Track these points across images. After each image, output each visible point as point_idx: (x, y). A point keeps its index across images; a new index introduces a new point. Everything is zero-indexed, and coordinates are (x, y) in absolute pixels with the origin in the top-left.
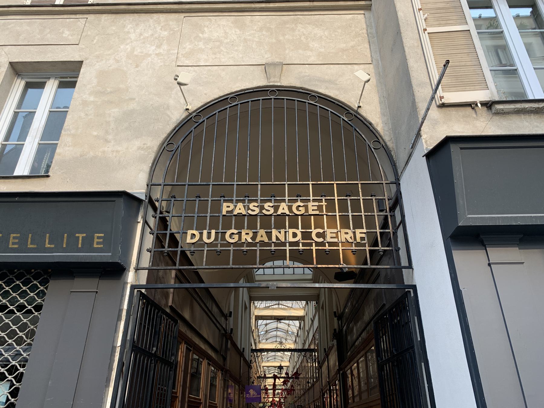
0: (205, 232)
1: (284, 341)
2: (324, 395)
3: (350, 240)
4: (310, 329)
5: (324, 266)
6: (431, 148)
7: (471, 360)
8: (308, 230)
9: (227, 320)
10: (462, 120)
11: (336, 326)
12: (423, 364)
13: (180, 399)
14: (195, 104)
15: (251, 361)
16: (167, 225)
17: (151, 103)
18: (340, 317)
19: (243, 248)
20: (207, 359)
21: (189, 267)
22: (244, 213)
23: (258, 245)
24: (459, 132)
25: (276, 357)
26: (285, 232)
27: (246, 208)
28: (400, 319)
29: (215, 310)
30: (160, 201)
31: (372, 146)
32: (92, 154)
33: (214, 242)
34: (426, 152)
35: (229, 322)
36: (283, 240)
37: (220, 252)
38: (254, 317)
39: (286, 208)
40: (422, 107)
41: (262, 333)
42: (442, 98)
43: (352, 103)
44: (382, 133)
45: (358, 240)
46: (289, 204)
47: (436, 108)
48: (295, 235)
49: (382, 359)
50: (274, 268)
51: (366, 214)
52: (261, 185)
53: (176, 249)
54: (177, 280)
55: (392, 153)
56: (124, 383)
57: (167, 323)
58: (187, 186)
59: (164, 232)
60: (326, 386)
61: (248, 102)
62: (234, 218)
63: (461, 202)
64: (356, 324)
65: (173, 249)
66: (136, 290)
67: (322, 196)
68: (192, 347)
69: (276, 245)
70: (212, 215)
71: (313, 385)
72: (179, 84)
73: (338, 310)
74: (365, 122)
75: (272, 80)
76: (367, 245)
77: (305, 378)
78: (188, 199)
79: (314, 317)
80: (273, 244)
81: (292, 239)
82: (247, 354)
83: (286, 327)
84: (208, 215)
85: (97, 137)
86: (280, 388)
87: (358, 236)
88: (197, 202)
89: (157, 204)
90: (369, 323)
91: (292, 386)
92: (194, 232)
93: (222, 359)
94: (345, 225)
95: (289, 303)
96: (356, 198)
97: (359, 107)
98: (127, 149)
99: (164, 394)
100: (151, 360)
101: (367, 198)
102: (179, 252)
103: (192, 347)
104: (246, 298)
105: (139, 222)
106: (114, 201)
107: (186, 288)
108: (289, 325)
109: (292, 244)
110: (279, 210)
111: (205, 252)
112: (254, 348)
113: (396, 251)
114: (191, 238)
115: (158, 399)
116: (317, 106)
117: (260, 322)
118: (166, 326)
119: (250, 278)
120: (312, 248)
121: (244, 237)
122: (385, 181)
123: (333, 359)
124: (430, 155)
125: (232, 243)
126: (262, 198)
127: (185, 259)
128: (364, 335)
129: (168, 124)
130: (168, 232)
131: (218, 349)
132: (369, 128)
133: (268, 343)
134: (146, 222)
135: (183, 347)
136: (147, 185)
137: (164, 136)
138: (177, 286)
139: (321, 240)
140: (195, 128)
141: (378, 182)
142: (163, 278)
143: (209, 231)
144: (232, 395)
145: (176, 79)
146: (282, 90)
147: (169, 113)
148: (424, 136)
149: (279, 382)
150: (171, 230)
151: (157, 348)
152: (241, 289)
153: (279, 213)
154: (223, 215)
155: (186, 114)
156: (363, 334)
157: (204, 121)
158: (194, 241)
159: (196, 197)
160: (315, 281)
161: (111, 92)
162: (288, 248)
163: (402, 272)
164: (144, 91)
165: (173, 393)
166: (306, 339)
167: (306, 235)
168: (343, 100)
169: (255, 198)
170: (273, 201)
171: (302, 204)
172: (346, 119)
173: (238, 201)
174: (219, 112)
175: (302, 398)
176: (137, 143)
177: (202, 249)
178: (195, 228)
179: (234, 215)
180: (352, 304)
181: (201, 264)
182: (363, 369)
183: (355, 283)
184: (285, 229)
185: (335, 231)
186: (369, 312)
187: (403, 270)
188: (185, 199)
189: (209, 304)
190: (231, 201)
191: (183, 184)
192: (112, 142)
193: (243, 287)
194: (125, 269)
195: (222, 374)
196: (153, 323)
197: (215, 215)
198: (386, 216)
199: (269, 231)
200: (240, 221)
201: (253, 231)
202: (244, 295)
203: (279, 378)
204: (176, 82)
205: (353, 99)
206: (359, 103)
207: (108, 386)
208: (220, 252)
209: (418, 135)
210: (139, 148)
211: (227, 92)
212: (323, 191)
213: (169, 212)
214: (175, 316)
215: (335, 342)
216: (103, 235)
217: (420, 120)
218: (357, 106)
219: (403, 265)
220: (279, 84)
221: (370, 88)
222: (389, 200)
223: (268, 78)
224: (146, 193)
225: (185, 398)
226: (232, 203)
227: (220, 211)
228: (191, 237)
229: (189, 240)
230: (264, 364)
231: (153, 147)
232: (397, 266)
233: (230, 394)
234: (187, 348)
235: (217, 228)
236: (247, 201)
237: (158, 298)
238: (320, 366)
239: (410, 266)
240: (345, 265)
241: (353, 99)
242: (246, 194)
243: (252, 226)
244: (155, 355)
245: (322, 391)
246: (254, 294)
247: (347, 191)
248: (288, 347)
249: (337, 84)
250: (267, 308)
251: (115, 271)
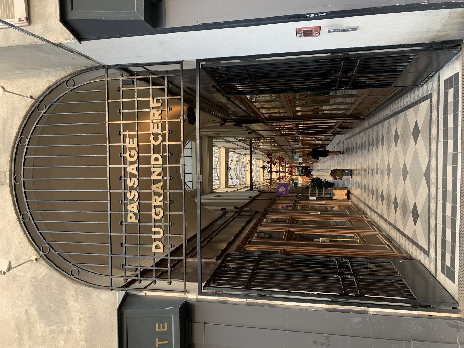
0: (154, 237)
1: (244, 165)
2: (283, 135)
3: (160, 112)
4: (235, 144)
5: (182, 136)
6: (72, 36)
7: (253, 23)
8: (152, 148)
9: (227, 212)
10: (43, 4)
11: (232, 124)
12: (257, 59)
13: (285, 247)
14: (30, 252)
15: (259, 191)
16: (148, 269)
17: (30, 294)
18: (225, 121)
19: (168, 204)
20: (257, 227)
21: (184, 248)
22: (137, 204)
23: (165, 191)
24: (56, 7)
25: (256, 170)
26: (154, 167)
27: (132, 202)
28: (223, 74)
29: (220, 222)
30: (126, 278)
31: (72, 88)
32: (82, 343)
33: (163, 228)
34: (76, 40)
35: (229, 210)
36: (161, 169)
37: (172, 223)
38: (226, 189)
39: (132, 167)
40: (30, 40)
41: (238, 182)
42: (20, 20)
43: (27, 104)
44: (59, 78)
45: (159, 105)
46: (128, 164)
48: (156, 159)
49: (254, 91)
50: (184, 174)
51: (136, 96)
52: (110, 189)
53: (169, 261)
54: (195, 257)
55: (79, 69)
56: (273, 293)
57: (229, 262)
58: (112, 256)
59: (154, 272)
60: (276, 133)
61: (27, 202)
62: (141, 213)
63: (123, 15)
64: (229, 109)
65: (169, 263)
67: (120, 135)
68: (247, 240)
69: (165, 175)
70: (139, 232)
71: (276, 142)
72: (9, 269)
73: (219, 122)
74: (48, 92)
75: (3, 180)
76: (163, 98)
77: (271, 148)
78: (124, 253)
79: (225, 140)
80: (165, 178)
81: (160, 162)
82: (254, 194)
83: (234, 163)
84: (139, 235)
85: (66, 340)
86: (278, 167)
87: (155, 105)
88: (127, 245)
89: (129, 280)
90: (228, 98)
91: (277, 159)
92: (154, 246)
93: (257, 215)
94: (146, 115)
95: (215, 161)
96: (121, 104)
97: (31, 97)
98: (77, 312)
99: (282, 260)
100: (257, 273)
101: (121, 95)
102: (172, 258)
103: (247, 240)
104: (211, 196)
105: (146, 294)
106: (127, 318)
107: (201, 248)
108: (232, 161)
109: (164, 162)
110: (133, 173)
111: (171, 235)
112: (249, 188)
113: (168, 73)
114: (160, 248)
115: (285, 265)
116: (31, 137)
117: (230, 184)
118: (232, 262)
119: (193, 194)
120: (167, 145)
121: (158, 203)
122: (105, 78)
123: (256, 127)
124: (80, 38)
125: (164, 213)
126: (123, 188)
127: (176, 252)
128: (237, 103)
129: (52, 276)
130: (154, 268)
131: (249, 218)
132: (54, 89)
134: (146, 288)
135: (248, 247)
136: (112, 290)
137: (64, 279)
138: (199, 257)
139: (160, 137)
140: (56, 251)
141: (106, 84)
142: (193, 268)
143: (153, 233)
144: (284, 205)
145: (4, 273)
146: (14, 170)
147: (40, 277)
148: (60, 40)
149: (274, 168)
150: (152, 266)
151: (248, 269)
152: (202, 201)
153: (136, 173)
154: (139, 222)
155: (42, 262)
156: (236, 103)
157: (48, 243)
158: (162, 246)
159: (122, 246)
160: (195, 140)
161: (19, 333)
162: (167, 165)
163: (186, 70)
164: (17, 302)
165: (281, 254)
166: (243, 147)
167: (156, 149)
168: (24, 112)
169: (123, 195)
170: (126, 178)
171: (128, 153)
172: (45, 110)
173: (126, 210)
174: (38, 230)
175: (286, 151)
176: (72, 303)
177: (169, 238)
178: (150, 246)
179: (139, 212)
180: (214, 111)
181: (181, 238)
182: (263, 103)
183: (195, 106)
184: (151, 167)
185: (152, 124)
186: (220, 98)
187: (184, 68)
188: (124, 256)
189: (215, 227)
190: (126, 216)
191: (110, 259)
192: (70, 326)
193: (200, 199)
194: (186, 302)
195: (268, 214)
196: (230, 274)
197: (138, 229)
198: (137, 79)
199: (153, 181)
200: (143, 208)
201: (153, 195)
202: (207, 199)
203: (271, 168)
205: (23, 103)
206: (27, 97)
207: (275, 306)
208: (172, 223)
209: (59, 45)
210: (77, 301)
211: (18, 223)
212: (115, 133)
213: (137, 269)
214: (223, 255)
215: (244, 125)
216: (157, 324)
217: (44, 42)
218: (31, 100)
219: (180, 69)
220: (8, 173)
221: (12, 86)
222: (122, 76)
224: (119, 290)
225: (285, 243)
226: (127, 214)
227: (135, 225)
228: (159, 249)
229: (161, 250)
230: (262, 180)
231: (75, 288)
232: (181, 74)
233: (282, 207)
234: (248, 244)
235: (151, 227)
236: (126, 202)
237: (210, 271)
238: (263, 137)
239: (181, 63)
240: (181, 118)
241: (23, 103)
242: (120, 202)
243: (149, 196)
244: (253, 270)
246: (208, 190)
247: (115, 112)
248: (248, 162)
249: (7, 118)
250: (219, 179)
251: (187, 311)
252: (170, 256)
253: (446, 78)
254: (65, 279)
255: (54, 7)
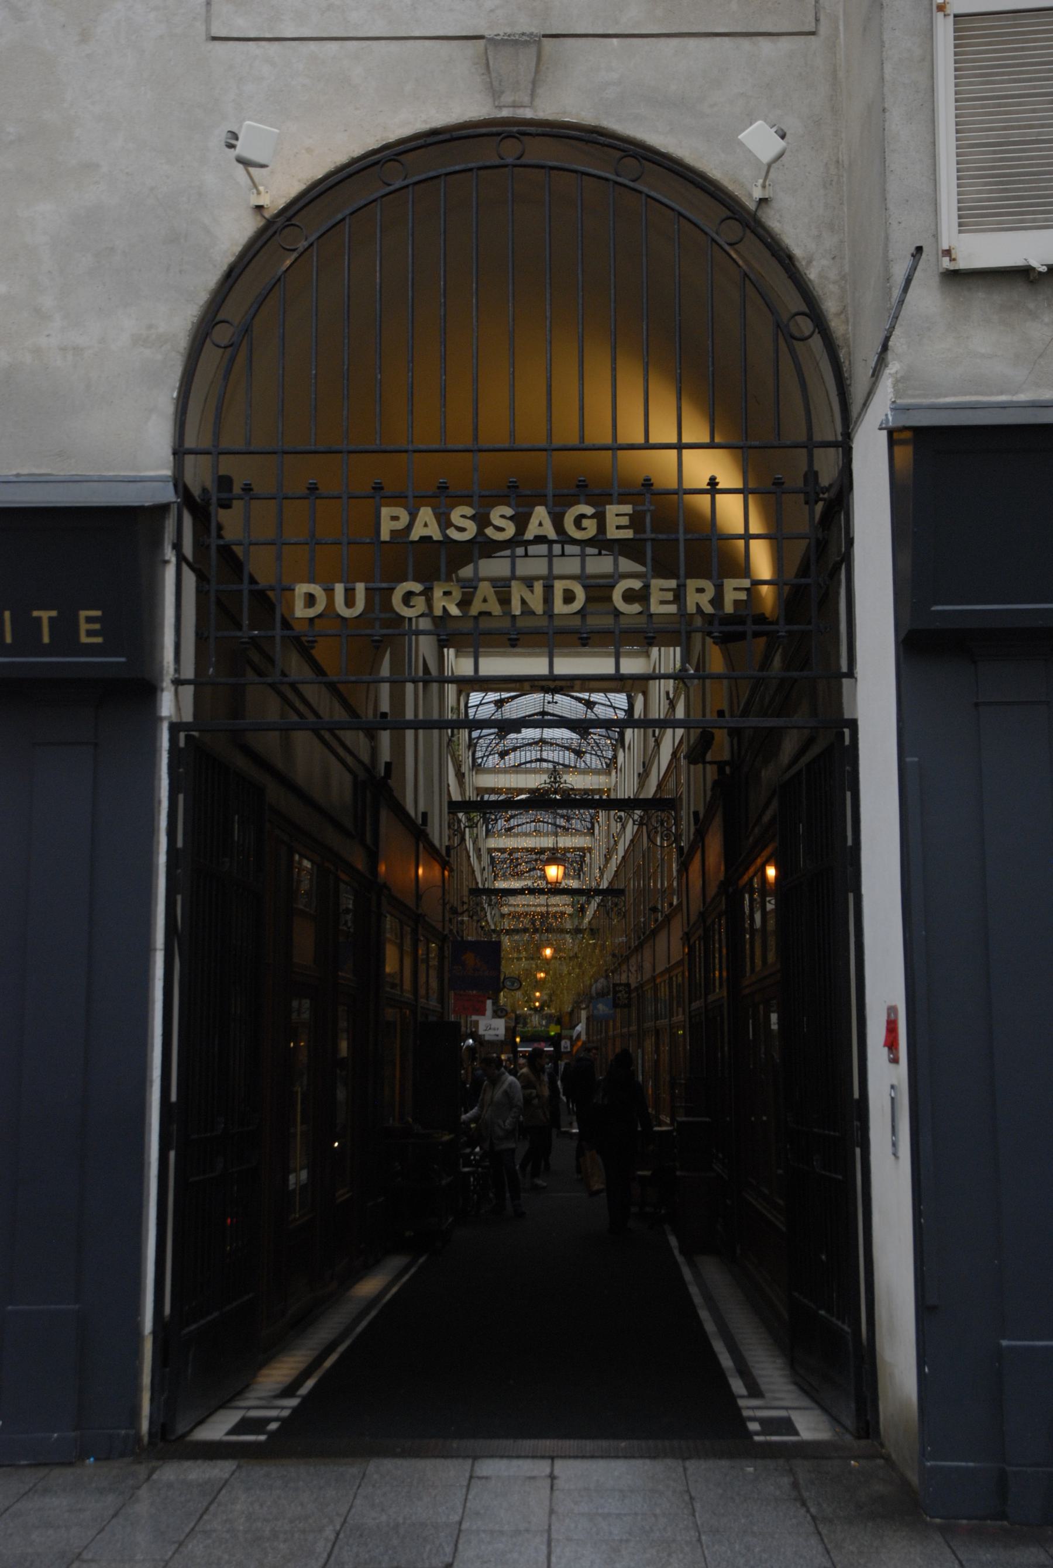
0: (339, 589)
14: (280, 189)
22: (437, 536)
46: (558, 509)
47: (935, 281)
66: (182, 735)
72: (240, 160)
92: (316, 589)
108: (590, 705)
112: (456, 797)
133: (505, 771)
143: (350, 585)
150: (253, 580)
158: (311, 613)
173: (422, 499)
175: (633, 961)
204: (232, 153)
223: (495, 93)
228: (306, 600)
239: (851, 674)
245: (689, 940)
252: (219, 547)
253: (793, 1418)
254: (202, 303)
255: (983, 351)
